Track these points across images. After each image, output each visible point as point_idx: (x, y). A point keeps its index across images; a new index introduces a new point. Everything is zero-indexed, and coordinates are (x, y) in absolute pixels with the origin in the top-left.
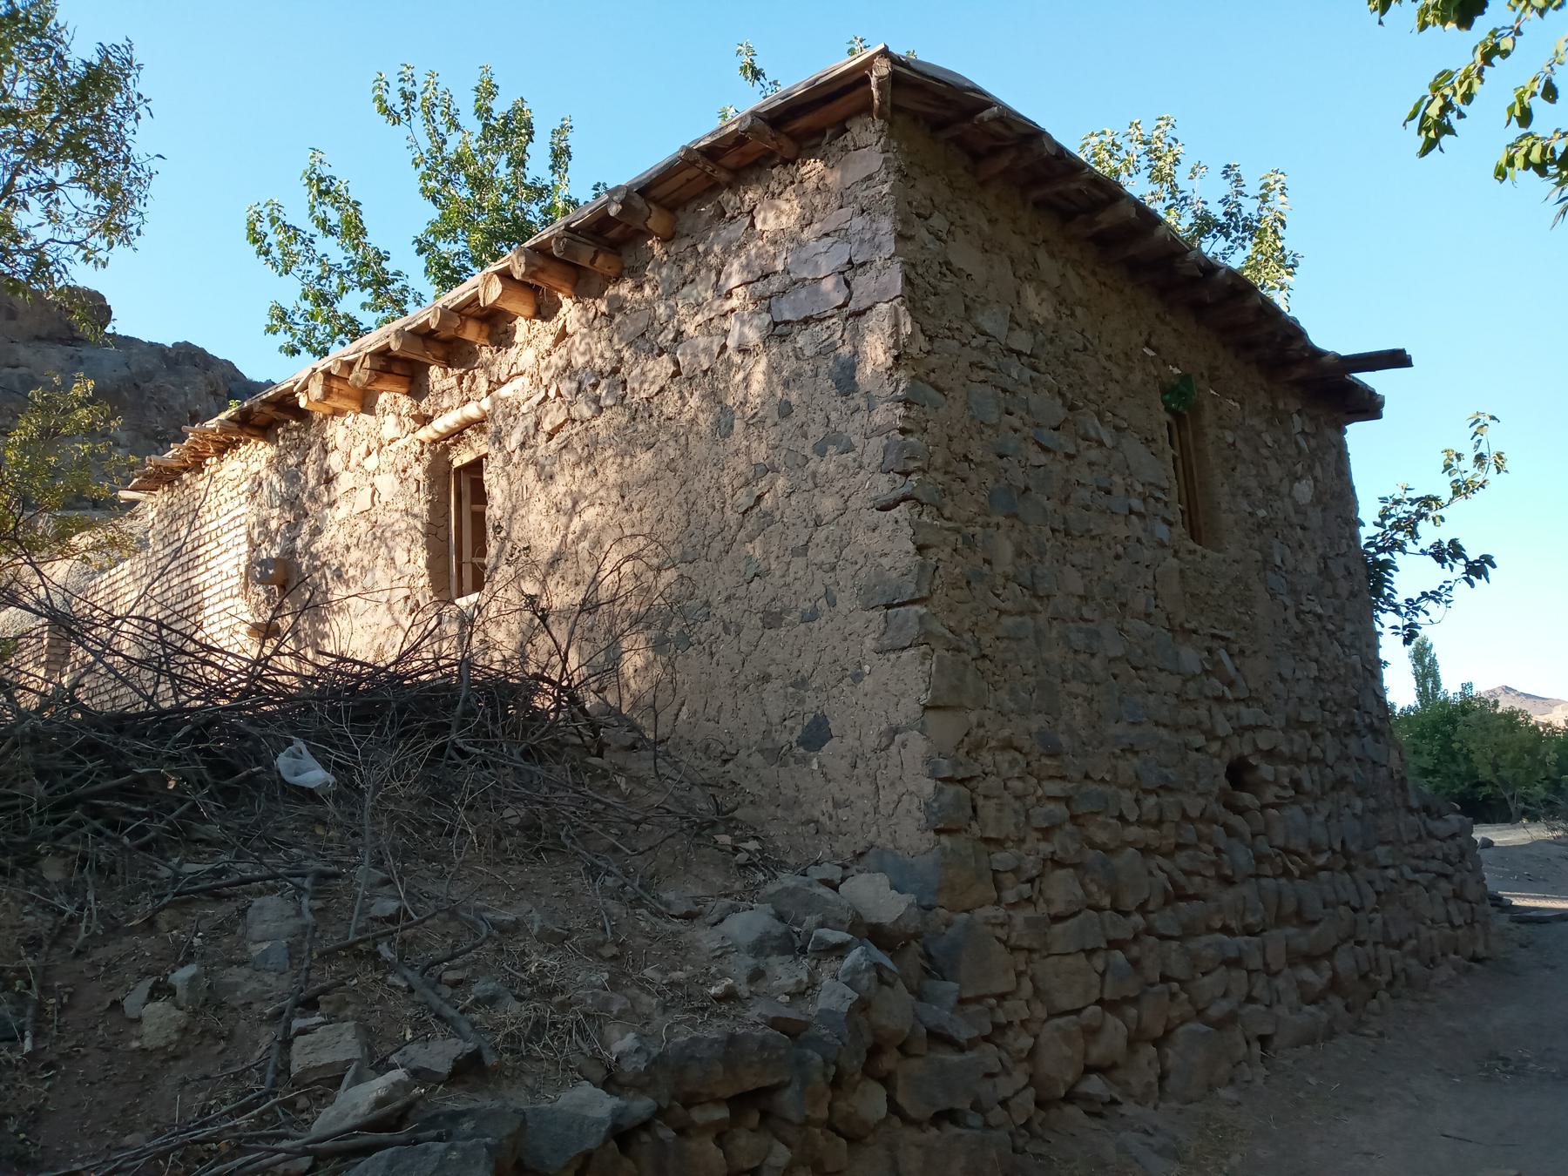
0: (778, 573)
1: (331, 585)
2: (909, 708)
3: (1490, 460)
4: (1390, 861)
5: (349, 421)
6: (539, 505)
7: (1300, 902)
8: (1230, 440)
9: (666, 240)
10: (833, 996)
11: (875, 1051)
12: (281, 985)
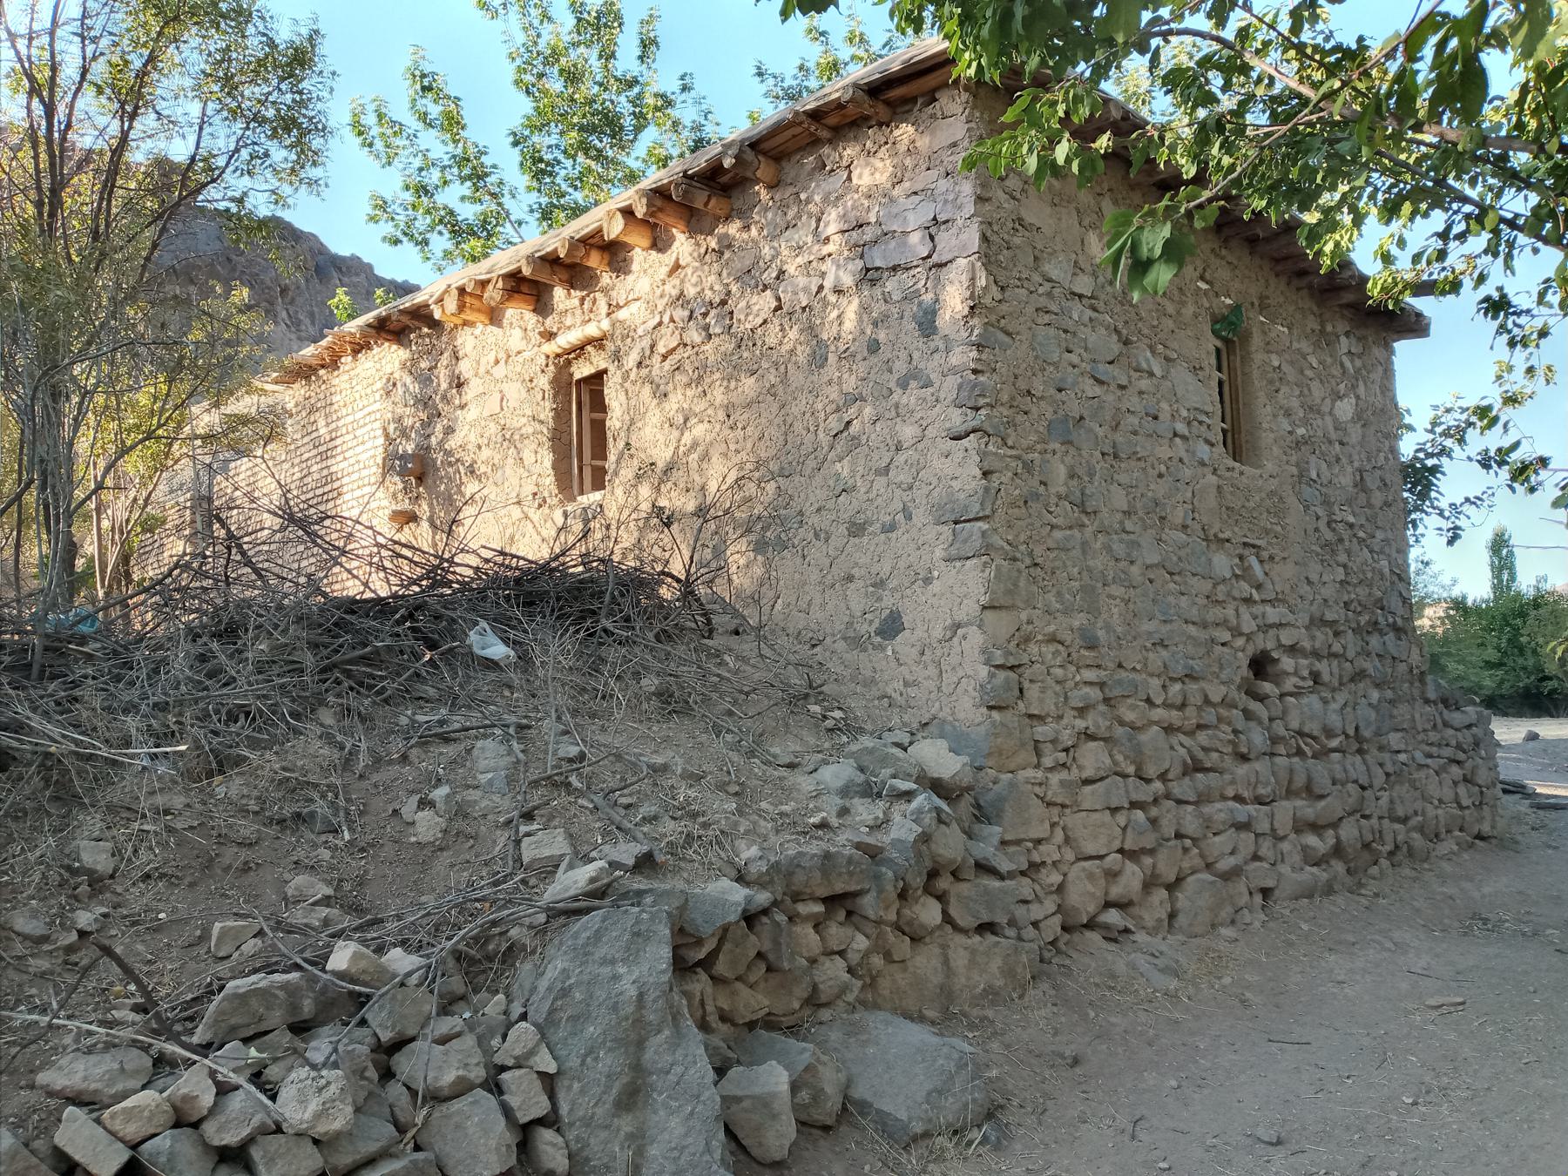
0: (863, 490)
1: (464, 479)
2: (970, 608)
3: (1540, 372)
4: (1403, 747)
5: (477, 331)
6: (654, 417)
7: (1310, 780)
8: (1276, 364)
9: (771, 187)
10: (903, 829)
11: (933, 874)
12: (507, 806)
